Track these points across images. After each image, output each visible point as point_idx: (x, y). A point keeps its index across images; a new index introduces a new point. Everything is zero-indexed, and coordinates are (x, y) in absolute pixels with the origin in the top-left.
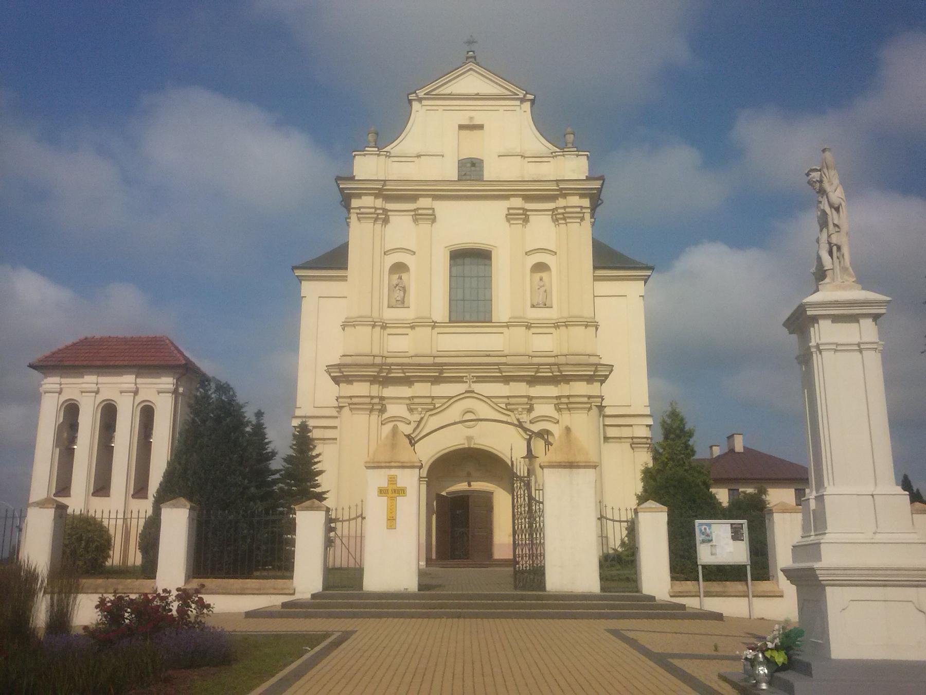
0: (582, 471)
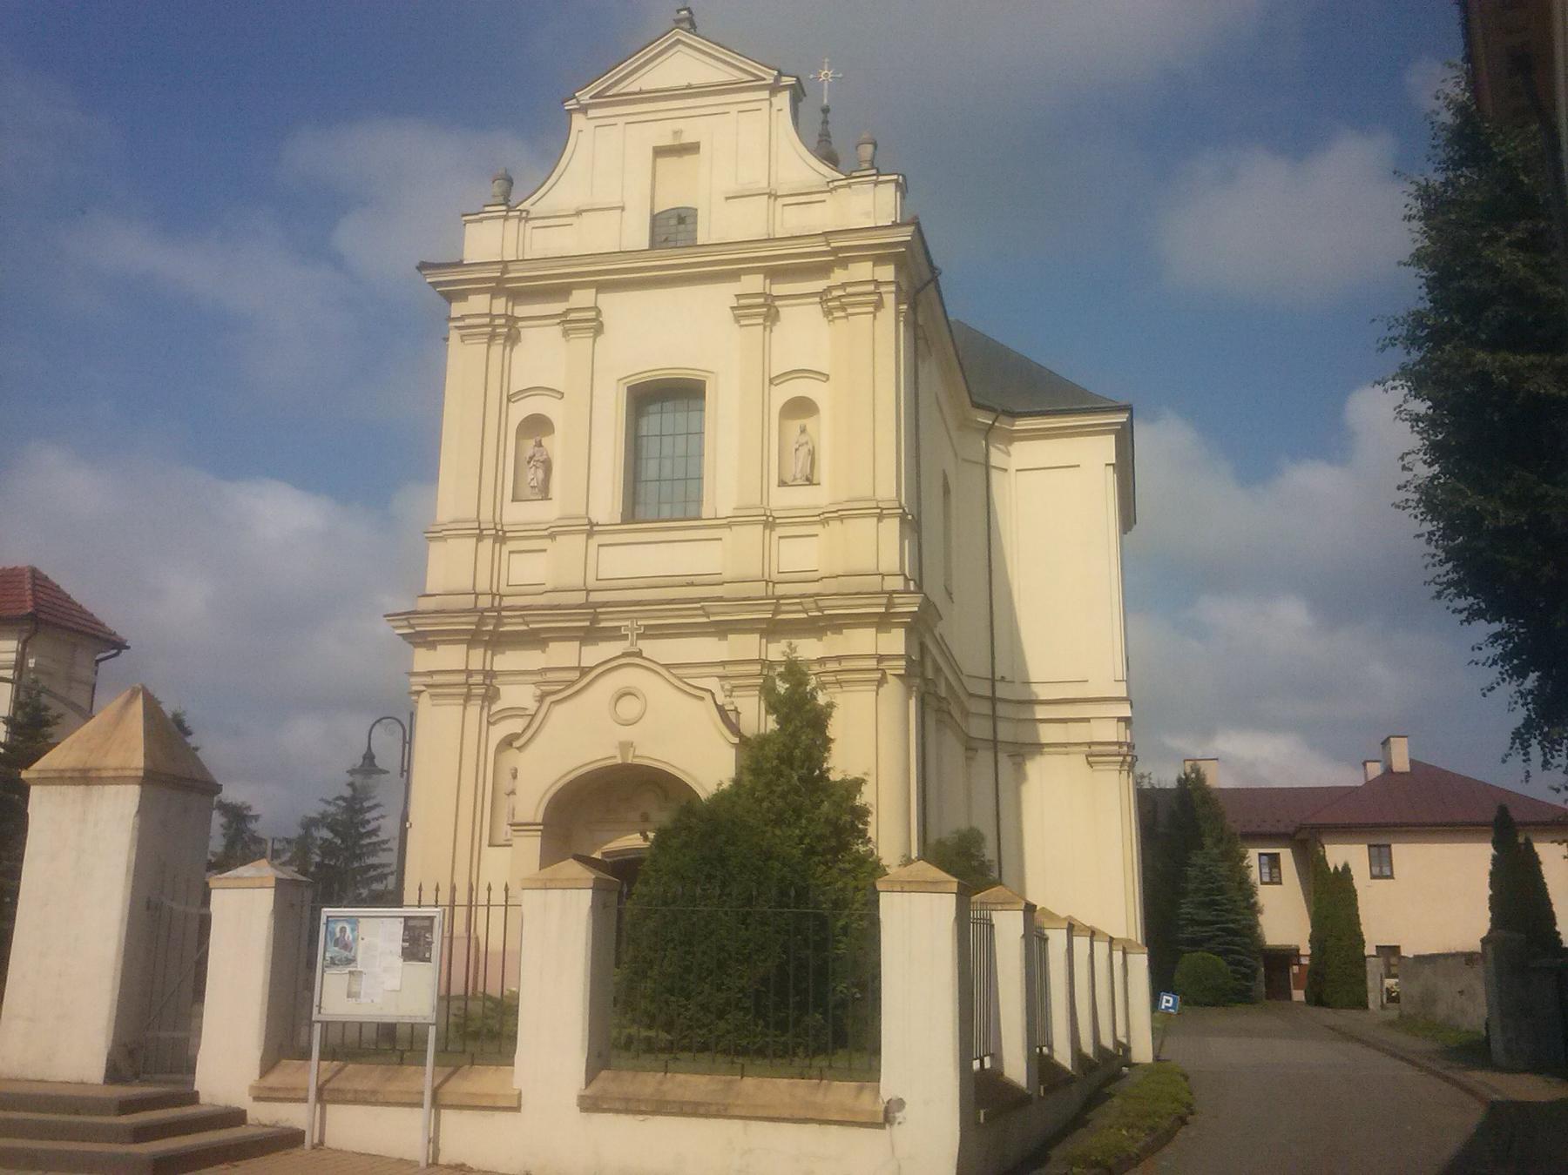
0: (111, 789)
